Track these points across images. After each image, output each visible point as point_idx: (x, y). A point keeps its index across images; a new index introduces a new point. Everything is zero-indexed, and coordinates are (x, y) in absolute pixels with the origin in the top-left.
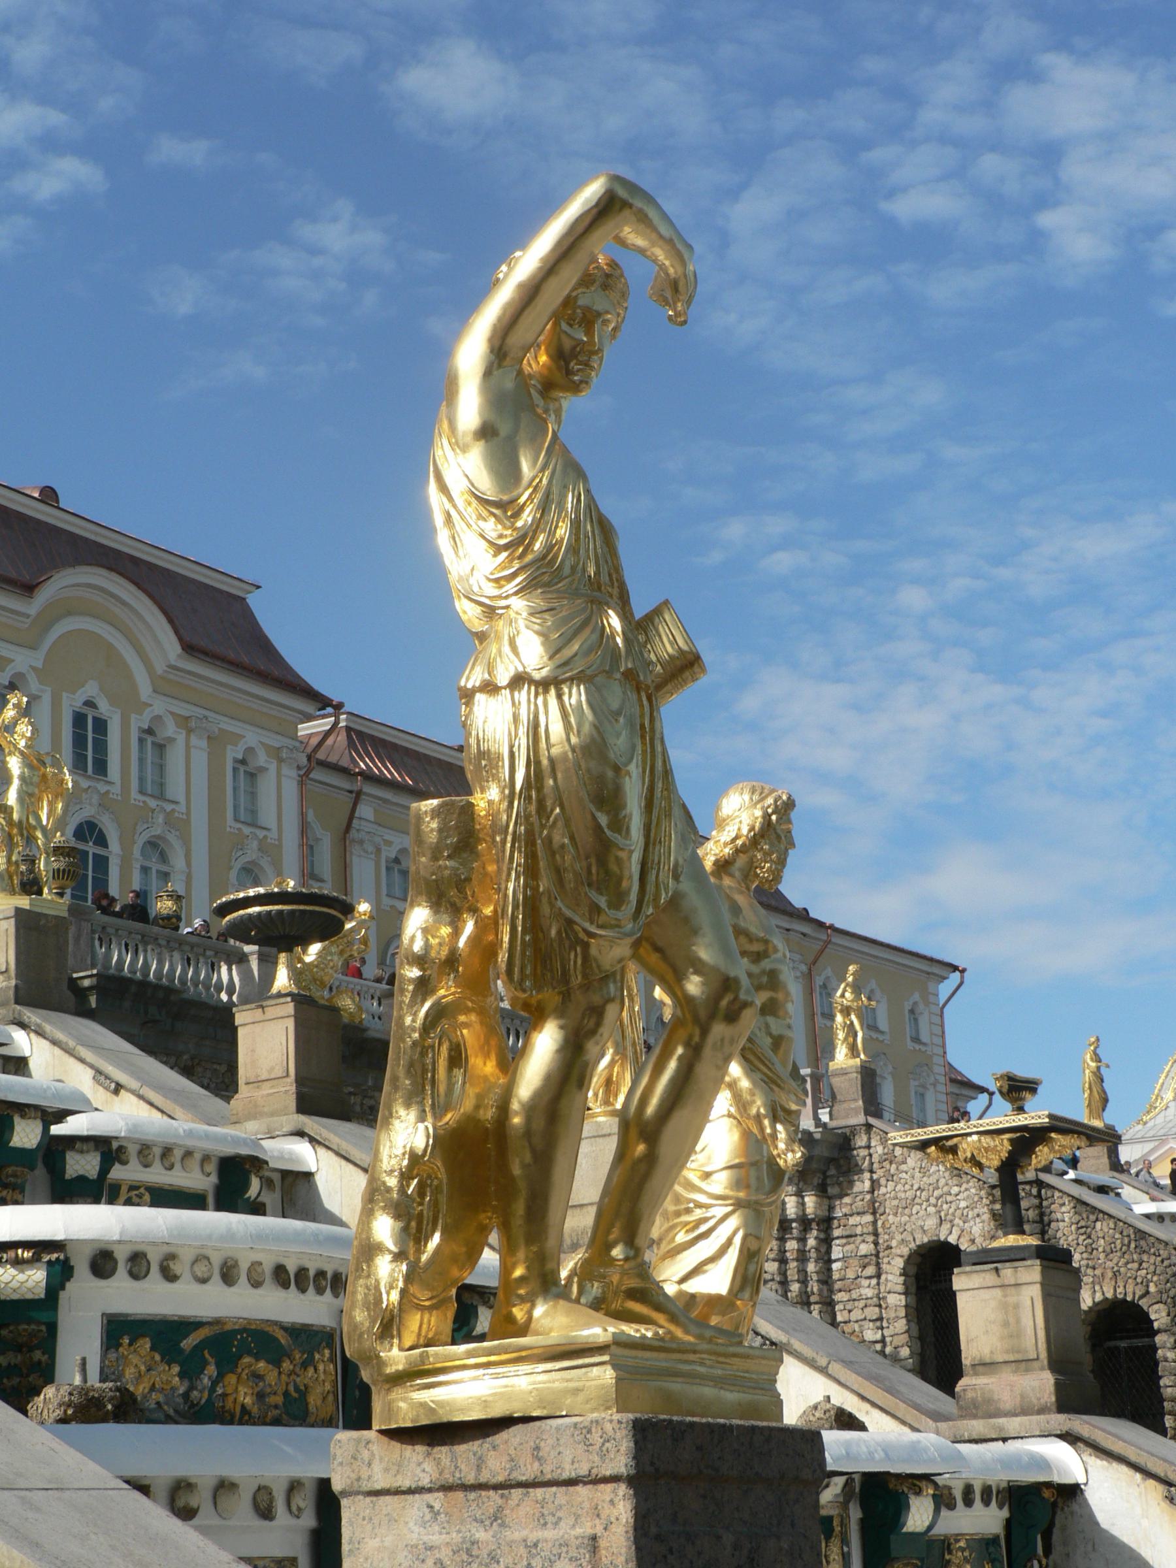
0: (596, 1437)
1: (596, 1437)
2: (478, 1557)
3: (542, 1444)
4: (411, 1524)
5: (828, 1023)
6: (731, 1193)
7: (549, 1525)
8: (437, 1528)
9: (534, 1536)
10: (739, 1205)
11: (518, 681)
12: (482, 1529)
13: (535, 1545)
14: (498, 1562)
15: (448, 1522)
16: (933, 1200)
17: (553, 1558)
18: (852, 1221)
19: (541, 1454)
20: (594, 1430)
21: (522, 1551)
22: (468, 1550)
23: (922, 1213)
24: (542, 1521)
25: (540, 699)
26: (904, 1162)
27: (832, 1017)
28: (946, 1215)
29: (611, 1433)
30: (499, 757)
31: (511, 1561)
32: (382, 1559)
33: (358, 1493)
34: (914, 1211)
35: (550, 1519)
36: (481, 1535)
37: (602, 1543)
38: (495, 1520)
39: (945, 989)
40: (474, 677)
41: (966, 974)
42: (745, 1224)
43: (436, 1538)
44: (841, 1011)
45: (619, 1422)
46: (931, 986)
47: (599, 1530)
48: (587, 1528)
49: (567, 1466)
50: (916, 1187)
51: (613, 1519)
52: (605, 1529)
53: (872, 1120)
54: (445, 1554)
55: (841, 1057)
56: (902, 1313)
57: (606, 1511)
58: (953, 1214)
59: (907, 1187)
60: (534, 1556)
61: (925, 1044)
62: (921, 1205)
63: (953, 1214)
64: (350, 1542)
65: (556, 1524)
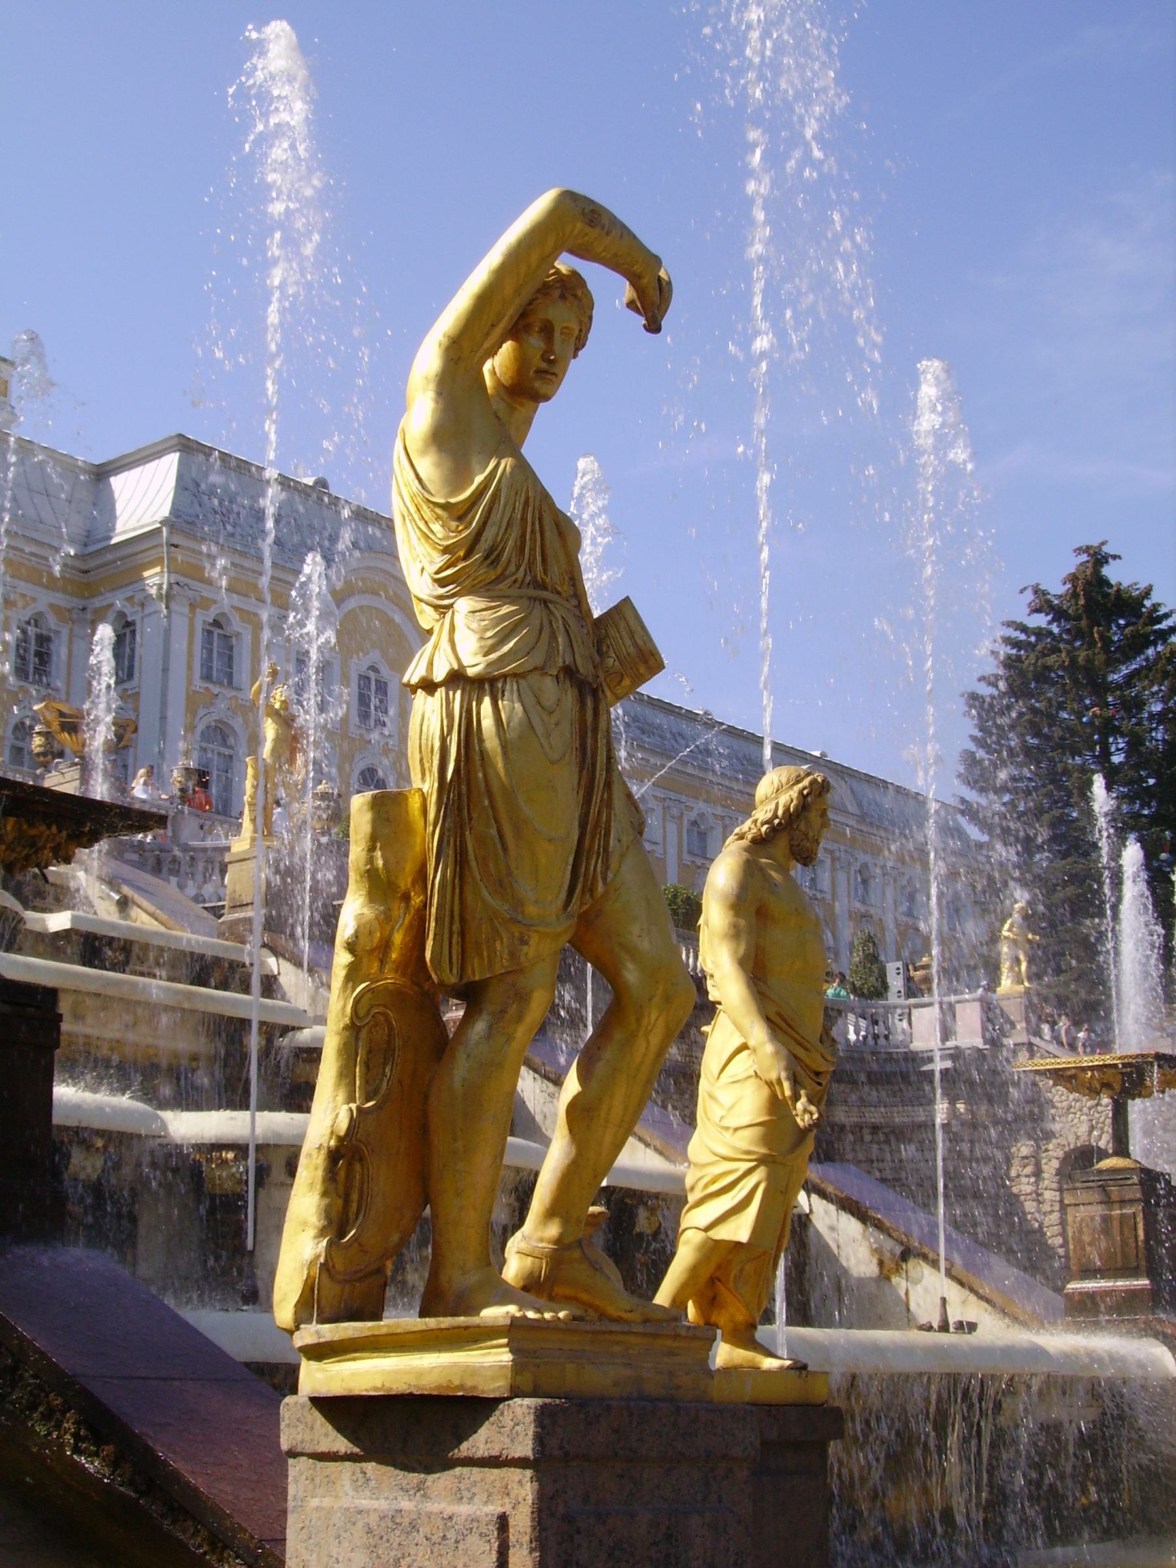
4: (347, 1488)
6: (756, 1149)
8: (369, 1494)
9: (450, 1509)
10: (762, 1161)
11: (456, 678)
12: (406, 1498)
13: (450, 1518)
21: (440, 1523)
23: (1076, 1121)
28: (1097, 1123)
29: (521, 1418)
32: (320, 1518)
33: (302, 1454)
35: (465, 1493)
36: (406, 1504)
37: (511, 1522)
40: (415, 673)
42: (770, 1178)
43: (365, 1503)
45: (529, 1407)
47: (507, 1509)
48: (495, 1509)
49: (482, 1446)
51: (520, 1499)
53: (1036, 1041)
54: (373, 1520)
57: (515, 1490)
58: (1103, 1123)
63: (1103, 1123)
64: (295, 1499)
65: (471, 1499)
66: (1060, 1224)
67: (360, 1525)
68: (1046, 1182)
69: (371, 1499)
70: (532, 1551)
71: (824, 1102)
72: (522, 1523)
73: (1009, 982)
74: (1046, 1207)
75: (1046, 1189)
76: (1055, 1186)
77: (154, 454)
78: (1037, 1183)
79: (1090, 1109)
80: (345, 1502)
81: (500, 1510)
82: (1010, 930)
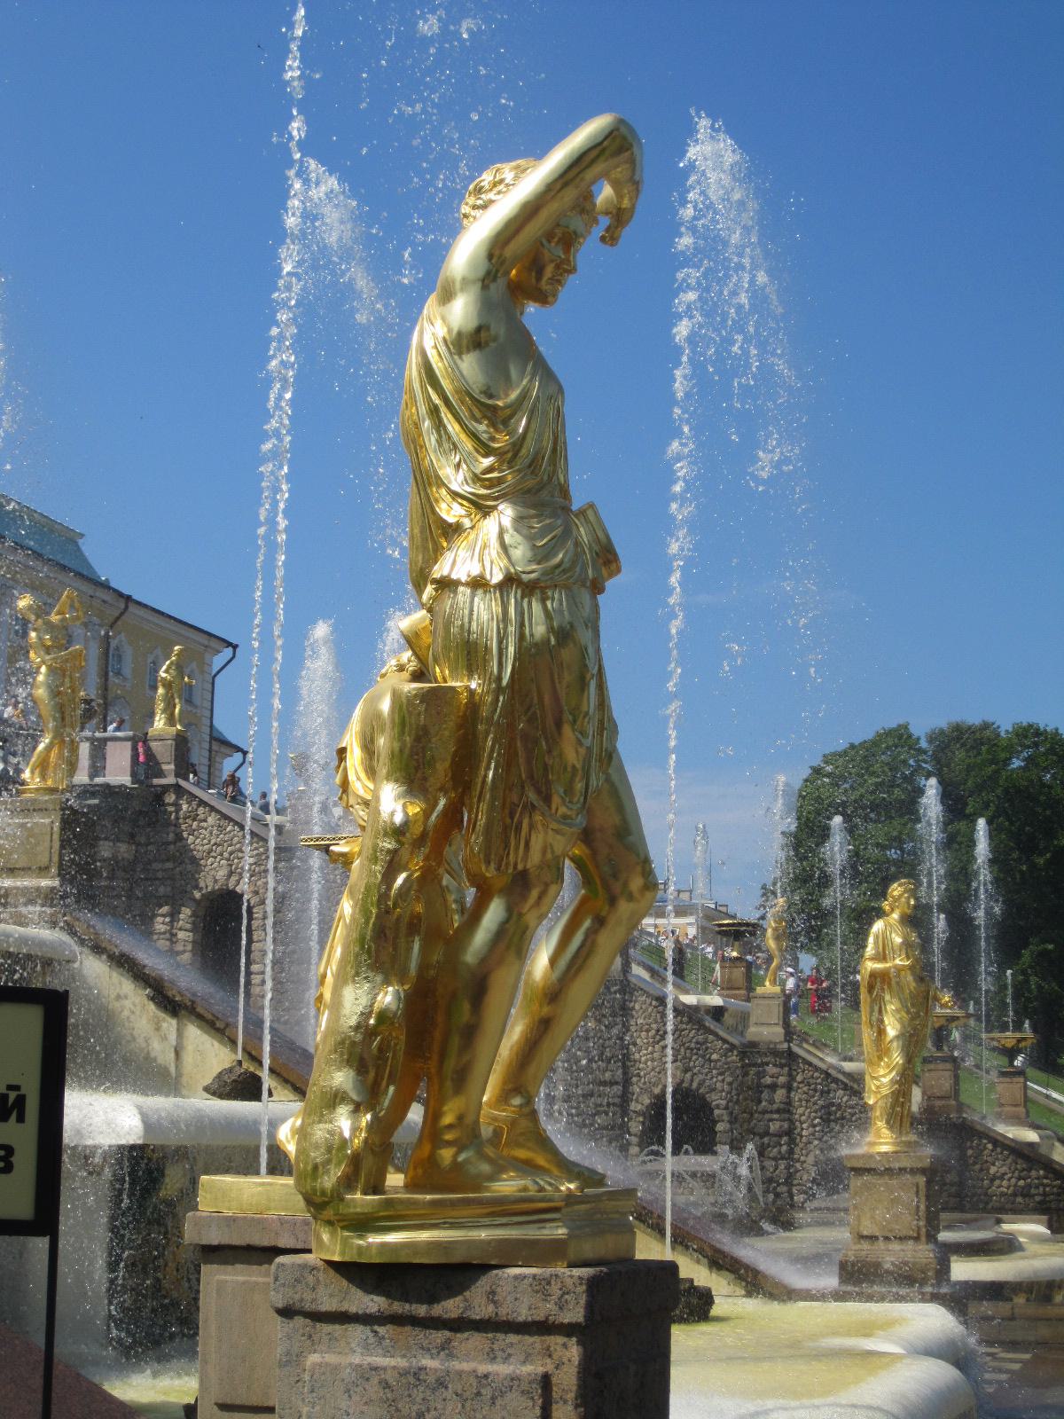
0: (555, 1289)
1: (555, 1289)
2: (425, 1381)
3: (499, 1290)
4: (353, 1345)
5: (152, 693)
7: (499, 1360)
9: (484, 1368)
12: (428, 1356)
14: (446, 1388)
15: (392, 1347)
16: (226, 855)
17: (504, 1389)
18: (156, 866)
19: (496, 1298)
20: (553, 1282)
22: (415, 1374)
24: (492, 1356)
25: (526, 600)
26: (205, 821)
27: (155, 688)
28: (236, 868)
30: (487, 649)
31: (460, 1387)
34: (209, 863)
35: (499, 1354)
36: (428, 1362)
37: (554, 1380)
38: (443, 1349)
39: (218, 661)
41: (238, 650)
44: (164, 686)
46: (207, 656)
47: (550, 1368)
50: (212, 842)
51: (565, 1360)
52: (557, 1368)
53: (182, 783)
54: (390, 1377)
55: (159, 723)
56: (189, 947)
57: (559, 1352)
59: (205, 841)
60: (484, 1386)
61: (196, 707)
62: (216, 858)
66: (251, 973)
67: (375, 1381)
68: (181, 922)
69: (385, 1356)
70: (576, 1406)
71: (669, 955)
72: (567, 1379)
73: (162, 722)
74: (179, 947)
75: (180, 929)
76: (189, 926)
77: (518, 231)
78: (172, 922)
79: (231, 854)
80: (357, 1359)
81: (541, 1370)
82: (166, 671)
